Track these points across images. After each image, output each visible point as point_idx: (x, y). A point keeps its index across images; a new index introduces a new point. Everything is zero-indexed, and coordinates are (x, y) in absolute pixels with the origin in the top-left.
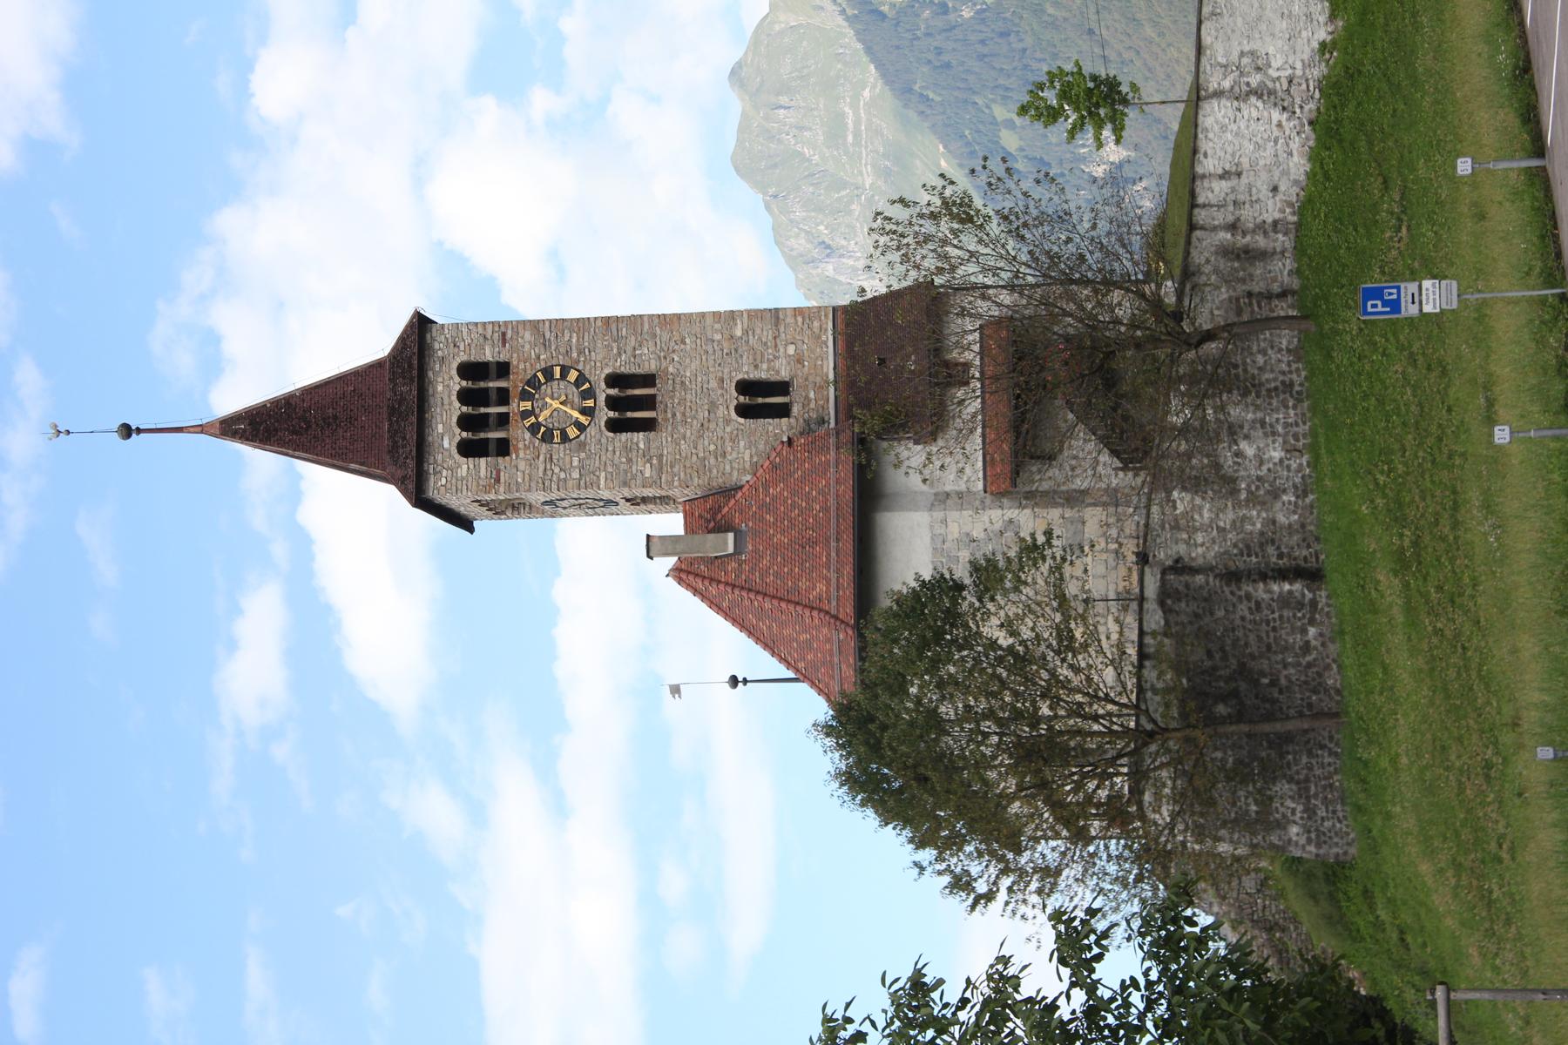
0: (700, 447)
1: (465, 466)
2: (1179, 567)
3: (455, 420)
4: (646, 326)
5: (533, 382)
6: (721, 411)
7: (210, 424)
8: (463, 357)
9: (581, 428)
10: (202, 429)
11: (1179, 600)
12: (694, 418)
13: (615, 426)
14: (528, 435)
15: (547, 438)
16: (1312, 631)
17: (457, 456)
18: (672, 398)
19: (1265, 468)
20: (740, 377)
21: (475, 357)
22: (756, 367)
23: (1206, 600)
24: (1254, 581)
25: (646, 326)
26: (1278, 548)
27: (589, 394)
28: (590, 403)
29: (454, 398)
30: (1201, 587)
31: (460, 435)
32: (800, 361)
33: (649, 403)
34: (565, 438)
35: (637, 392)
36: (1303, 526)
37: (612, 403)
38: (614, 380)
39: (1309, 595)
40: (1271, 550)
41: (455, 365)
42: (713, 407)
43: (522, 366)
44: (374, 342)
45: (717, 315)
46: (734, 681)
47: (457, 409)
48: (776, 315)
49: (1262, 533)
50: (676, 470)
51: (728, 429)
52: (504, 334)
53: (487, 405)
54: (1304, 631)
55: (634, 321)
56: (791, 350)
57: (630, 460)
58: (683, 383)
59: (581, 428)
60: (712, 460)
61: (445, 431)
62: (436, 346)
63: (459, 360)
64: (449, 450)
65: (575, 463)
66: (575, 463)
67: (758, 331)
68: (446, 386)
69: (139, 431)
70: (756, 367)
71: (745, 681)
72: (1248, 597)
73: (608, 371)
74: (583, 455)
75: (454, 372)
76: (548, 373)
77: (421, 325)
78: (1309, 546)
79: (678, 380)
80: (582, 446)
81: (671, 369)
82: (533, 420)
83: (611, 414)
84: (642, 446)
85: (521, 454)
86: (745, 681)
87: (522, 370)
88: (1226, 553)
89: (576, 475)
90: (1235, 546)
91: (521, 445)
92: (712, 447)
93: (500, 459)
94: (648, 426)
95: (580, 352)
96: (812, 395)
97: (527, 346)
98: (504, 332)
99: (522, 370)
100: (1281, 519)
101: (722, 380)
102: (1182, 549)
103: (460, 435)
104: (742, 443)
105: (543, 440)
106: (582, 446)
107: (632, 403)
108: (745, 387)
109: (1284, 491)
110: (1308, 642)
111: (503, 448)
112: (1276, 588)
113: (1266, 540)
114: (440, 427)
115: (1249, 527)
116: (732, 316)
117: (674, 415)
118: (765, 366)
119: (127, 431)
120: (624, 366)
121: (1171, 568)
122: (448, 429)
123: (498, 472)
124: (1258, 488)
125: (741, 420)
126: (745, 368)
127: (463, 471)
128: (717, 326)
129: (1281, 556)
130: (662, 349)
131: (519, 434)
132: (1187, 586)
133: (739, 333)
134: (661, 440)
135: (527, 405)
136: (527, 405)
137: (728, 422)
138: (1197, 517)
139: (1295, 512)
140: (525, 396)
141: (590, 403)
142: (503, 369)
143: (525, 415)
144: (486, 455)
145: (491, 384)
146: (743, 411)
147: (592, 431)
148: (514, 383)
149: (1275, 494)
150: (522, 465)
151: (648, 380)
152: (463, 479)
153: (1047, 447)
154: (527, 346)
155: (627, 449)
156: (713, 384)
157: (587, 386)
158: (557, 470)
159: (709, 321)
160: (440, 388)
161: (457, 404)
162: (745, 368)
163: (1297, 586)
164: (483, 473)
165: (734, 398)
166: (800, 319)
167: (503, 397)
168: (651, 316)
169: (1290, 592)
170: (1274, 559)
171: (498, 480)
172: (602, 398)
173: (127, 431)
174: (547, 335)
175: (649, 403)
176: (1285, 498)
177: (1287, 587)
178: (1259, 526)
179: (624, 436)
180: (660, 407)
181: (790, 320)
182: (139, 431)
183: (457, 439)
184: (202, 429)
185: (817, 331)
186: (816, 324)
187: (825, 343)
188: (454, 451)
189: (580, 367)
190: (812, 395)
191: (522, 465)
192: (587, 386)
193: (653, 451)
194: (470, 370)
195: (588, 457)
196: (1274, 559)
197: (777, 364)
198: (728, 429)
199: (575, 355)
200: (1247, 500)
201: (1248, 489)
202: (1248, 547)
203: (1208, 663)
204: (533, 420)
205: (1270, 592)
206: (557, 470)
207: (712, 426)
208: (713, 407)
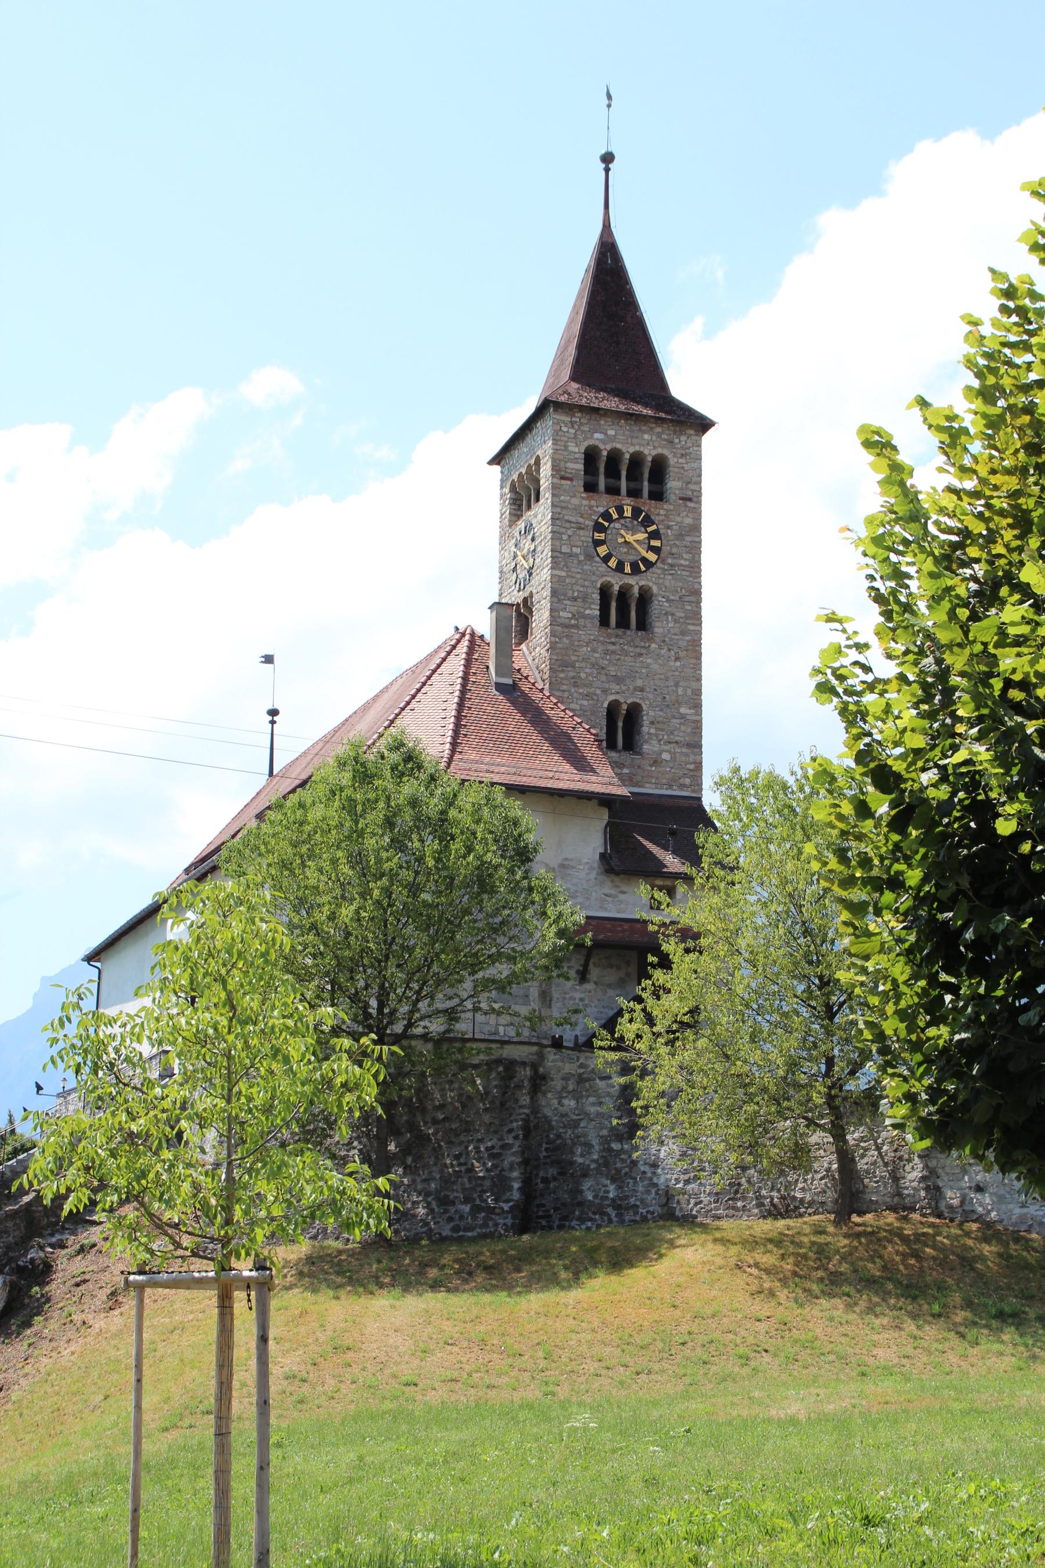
0: (583, 665)
1: (577, 450)
2: (539, 1081)
3: (619, 446)
4: (691, 628)
5: (648, 521)
6: (615, 687)
7: (611, 234)
8: (672, 460)
9: (606, 559)
10: (607, 227)
11: (502, 1078)
12: (610, 661)
13: (605, 592)
14: (601, 510)
15: (598, 528)
16: (467, 1208)
17: (586, 444)
18: (628, 644)
19: (647, 1168)
20: (645, 707)
21: (672, 471)
22: (652, 723)
23: (502, 1104)
24: (523, 1153)
25: (691, 628)
26: (555, 1179)
27: (635, 570)
28: (628, 569)
29: (637, 448)
30: (517, 1101)
31: (605, 449)
32: (656, 762)
33: (623, 623)
34: (598, 543)
35: (633, 614)
36: (580, 1204)
37: (624, 594)
38: (645, 599)
39: (506, 1207)
40: (552, 1172)
41: (666, 452)
42: (618, 680)
43: (662, 512)
44: (683, 385)
45: (698, 692)
46: (274, 713)
47: (628, 450)
48: (696, 746)
49: (572, 1163)
50: (565, 640)
51: (598, 692)
52: (690, 500)
53: (628, 479)
54: (467, 1200)
55: (696, 617)
56: (666, 756)
57: (575, 599)
58: (641, 655)
59: (606, 559)
60: (571, 674)
61: (610, 437)
62: (683, 438)
63: (670, 456)
64: (592, 437)
65: (574, 550)
66: (576, 550)
67: (683, 728)
68: (648, 443)
69: (607, 170)
70: (652, 723)
71: (273, 722)
72: (505, 1147)
73: (655, 589)
74: (582, 558)
75: (660, 451)
76: (655, 535)
77: (704, 425)
78: (556, 1209)
79: (644, 651)
80: (589, 557)
81: (653, 646)
82: (615, 516)
83: (616, 588)
84: (587, 612)
85: (585, 502)
86: (273, 722)
87: (658, 511)
88: (551, 1128)
89: (565, 549)
90: (559, 1136)
91: (593, 503)
92: (583, 675)
93: (582, 483)
94: (604, 621)
95: (672, 565)
96: (626, 771)
97: (679, 519)
98: (692, 499)
99: (658, 511)
100: (587, 1184)
101: (642, 690)
102: (557, 1084)
103: (605, 449)
104: (585, 703)
105: (597, 523)
106: (589, 557)
107: (626, 611)
108: (633, 714)
109: (620, 1187)
110: (453, 1203)
111: (590, 487)
112: (515, 1174)
113: (564, 1167)
114: (611, 432)
115: (579, 1150)
116: (698, 706)
117: (613, 644)
118: (653, 731)
119: (608, 159)
120: (658, 606)
121: (536, 1071)
122: (613, 439)
123: (571, 479)
124: (623, 1161)
125: (606, 705)
126: (651, 713)
127: (572, 447)
128: (689, 692)
129: (545, 1180)
130: (671, 639)
131: (602, 503)
132: (519, 1087)
133: (683, 710)
134: (592, 630)
135: (628, 513)
136: (628, 513)
137: (605, 691)
138: (592, 1099)
139: (596, 1197)
140: (636, 512)
141: (628, 569)
142: (658, 495)
143: (620, 510)
144: (586, 472)
145: (646, 483)
146: (612, 711)
147: (603, 568)
148: (647, 505)
149: (616, 1178)
150: (575, 501)
151: (643, 625)
152: (566, 447)
153: (594, 973)
154: (679, 519)
155: (585, 598)
156: (639, 683)
157: (643, 568)
158: (569, 532)
159: (694, 685)
160: (646, 437)
161: (632, 450)
162: (651, 713)
163: (516, 1195)
164: (570, 465)
165: (626, 700)
166: (692, 767)
167: (634, 493)
168: (700, 633)
169: (511, 1188)
170: (541, 1174)
171: (563, 478)
172: (631, 581)
173: (608, 159)
174: (688, 539)
175: (623, 623)
176: (612, 1188)
177: (516, 1185)
178: (580, 1160)
179: (596, 596)
180: (620, 632)
181: (692, 758)
182: (607, 170)
183: (601, 446)
184: (607, 227)
185: (681, 781)
186: (687, 781)
187: (670, 787)
188: (591, 442)
189: (659, 564)
190: (626, 771)
191: (575, 501)
192: (643, 568)
193: (582, 622)
194: (659, 469)
195: (580, 562)
196: (541, 1174)
197: (654, 742)
198: (598, 692)
199: (670, 561)
200: (610, 1150)
201: (622, 1151)
202: (556, 1149)
203: (429, 1105)
204: (615, 516)
205: (512, 1168)
206: (569, 532)
207: (603, 678)
208: (618, 680)
